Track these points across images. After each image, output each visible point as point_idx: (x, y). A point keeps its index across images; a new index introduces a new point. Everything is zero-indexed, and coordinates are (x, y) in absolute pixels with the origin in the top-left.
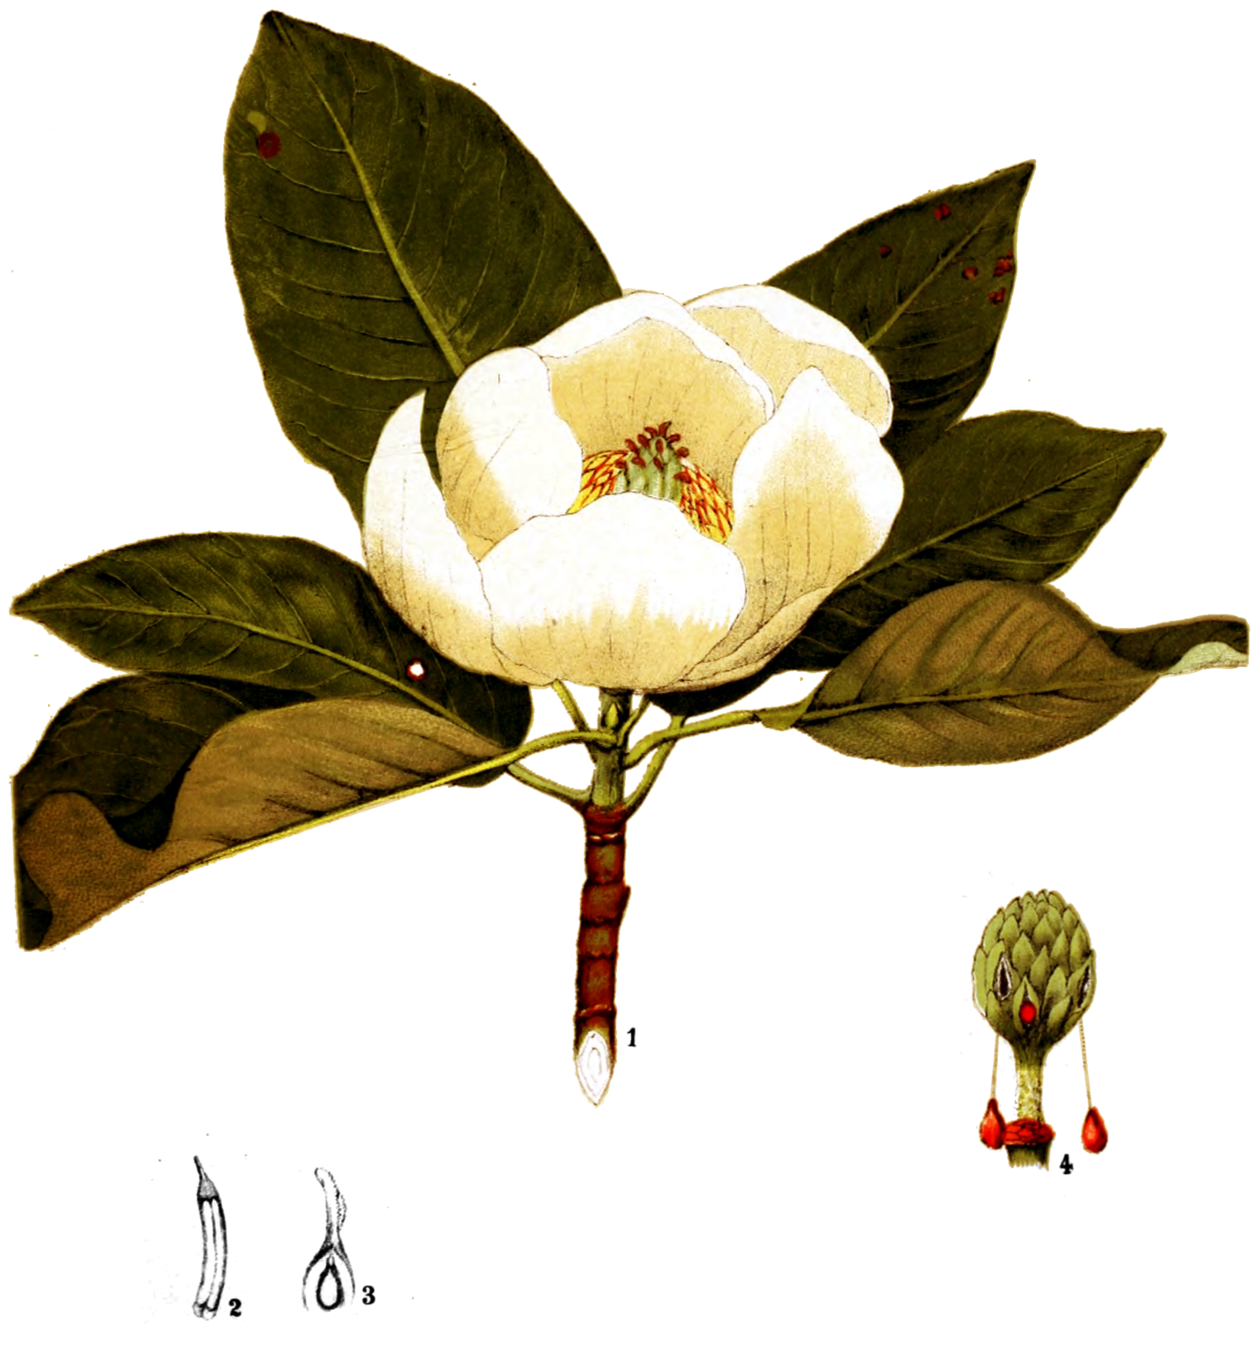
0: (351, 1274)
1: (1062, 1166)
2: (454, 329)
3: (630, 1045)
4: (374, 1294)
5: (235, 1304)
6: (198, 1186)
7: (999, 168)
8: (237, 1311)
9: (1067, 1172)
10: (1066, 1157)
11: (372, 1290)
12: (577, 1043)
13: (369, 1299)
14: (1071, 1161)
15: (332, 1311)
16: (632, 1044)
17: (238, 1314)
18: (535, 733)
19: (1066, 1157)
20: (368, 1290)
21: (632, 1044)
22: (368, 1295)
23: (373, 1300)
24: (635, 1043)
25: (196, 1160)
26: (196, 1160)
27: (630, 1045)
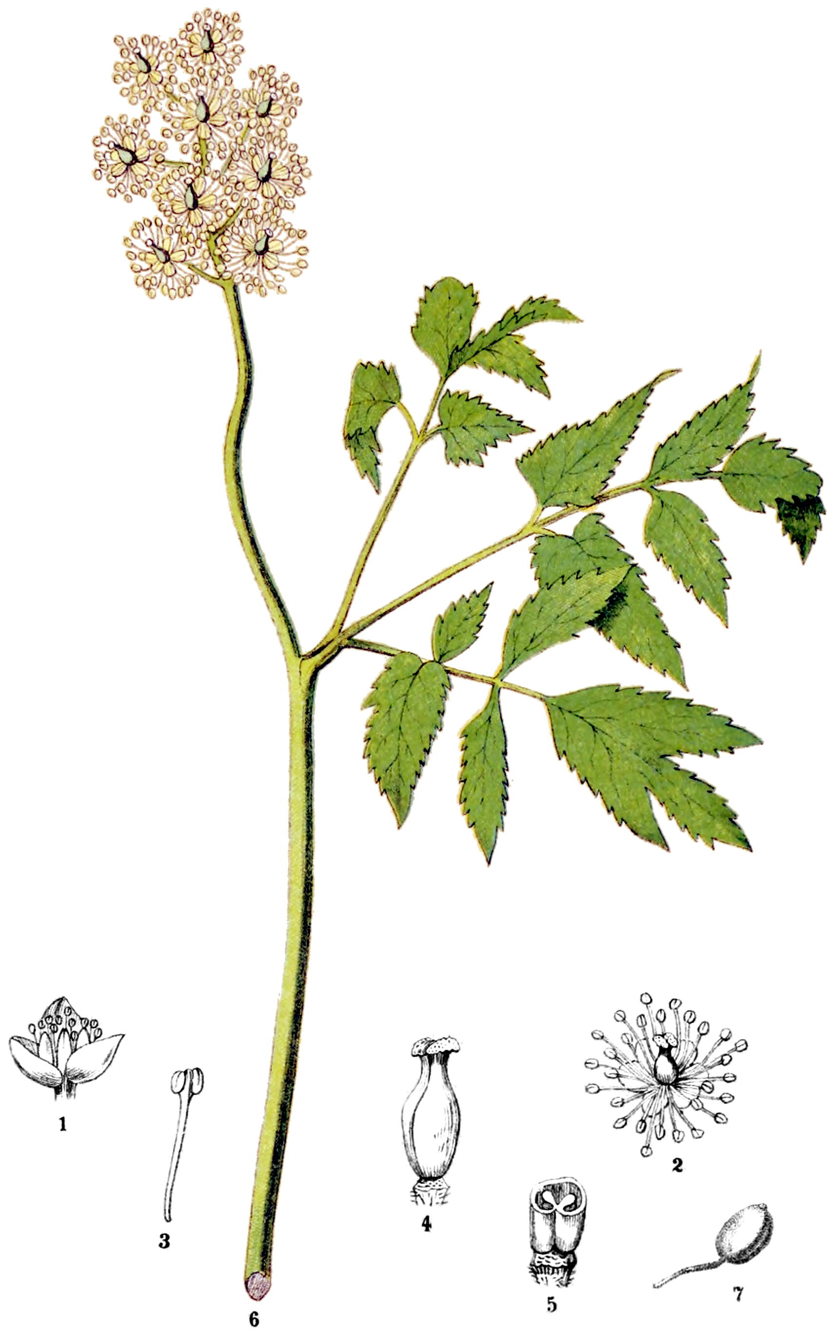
0: (414, 1115)
1: (423, 1225)
2: (209, 139)
3: (62, 1130)
4: (169, 1241)
5: (677, 1161)
6: (378, 622)
7: (432, 625)
8: (680, 1168)
9: (427, 1230)
10: (427, 1218)
11: (168, 1237)
12: (56, 1097)
13: (164, 1244)
14: (431, 1221)
15: (729, 1065)
16: (63, 1129)
17: (680, 1171)
18: (523, 550)
19: (427, 1218)
20: (164, 1236)
21: (63, 1129)
22: (164, 1240)
23: (168, 1245)
24: (66, 1128)
25: (678, 371)
26: (678, 371)
27: (62, 1130)
